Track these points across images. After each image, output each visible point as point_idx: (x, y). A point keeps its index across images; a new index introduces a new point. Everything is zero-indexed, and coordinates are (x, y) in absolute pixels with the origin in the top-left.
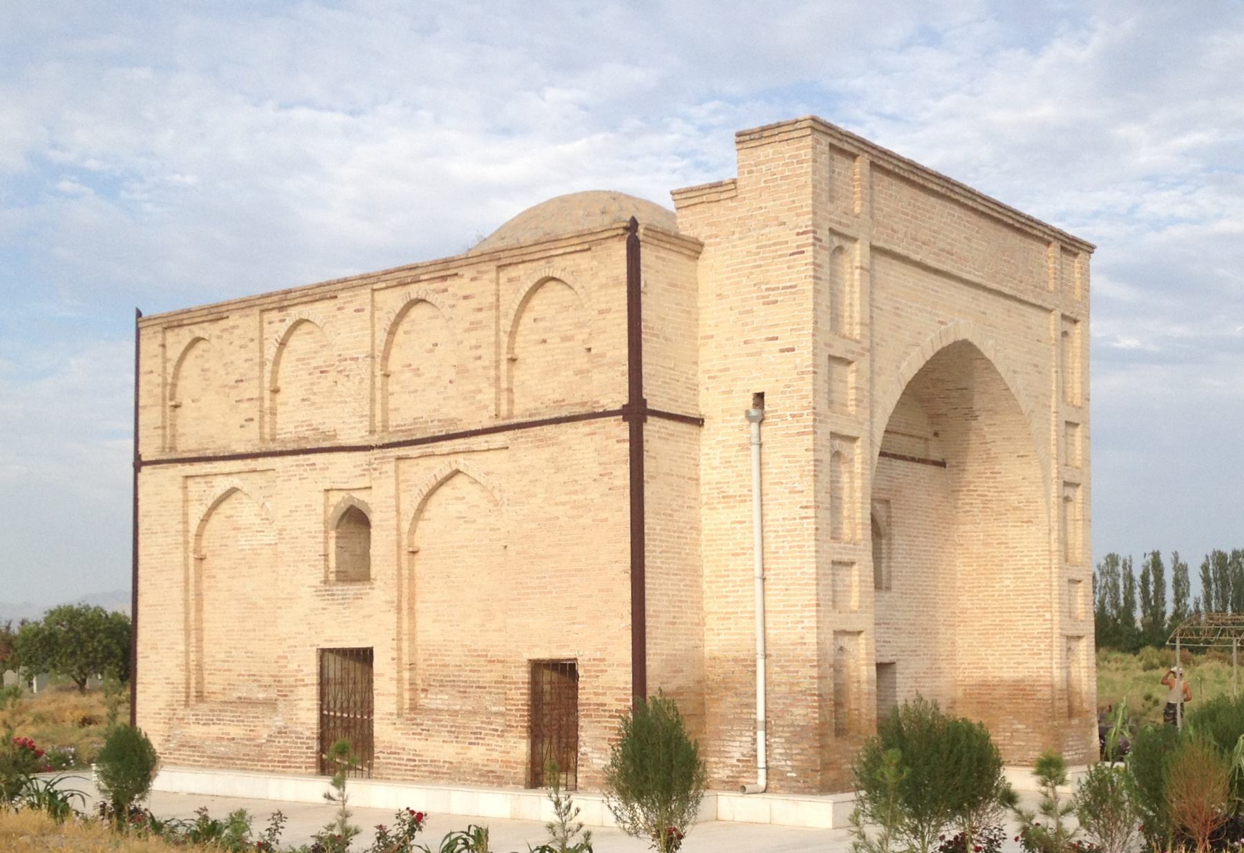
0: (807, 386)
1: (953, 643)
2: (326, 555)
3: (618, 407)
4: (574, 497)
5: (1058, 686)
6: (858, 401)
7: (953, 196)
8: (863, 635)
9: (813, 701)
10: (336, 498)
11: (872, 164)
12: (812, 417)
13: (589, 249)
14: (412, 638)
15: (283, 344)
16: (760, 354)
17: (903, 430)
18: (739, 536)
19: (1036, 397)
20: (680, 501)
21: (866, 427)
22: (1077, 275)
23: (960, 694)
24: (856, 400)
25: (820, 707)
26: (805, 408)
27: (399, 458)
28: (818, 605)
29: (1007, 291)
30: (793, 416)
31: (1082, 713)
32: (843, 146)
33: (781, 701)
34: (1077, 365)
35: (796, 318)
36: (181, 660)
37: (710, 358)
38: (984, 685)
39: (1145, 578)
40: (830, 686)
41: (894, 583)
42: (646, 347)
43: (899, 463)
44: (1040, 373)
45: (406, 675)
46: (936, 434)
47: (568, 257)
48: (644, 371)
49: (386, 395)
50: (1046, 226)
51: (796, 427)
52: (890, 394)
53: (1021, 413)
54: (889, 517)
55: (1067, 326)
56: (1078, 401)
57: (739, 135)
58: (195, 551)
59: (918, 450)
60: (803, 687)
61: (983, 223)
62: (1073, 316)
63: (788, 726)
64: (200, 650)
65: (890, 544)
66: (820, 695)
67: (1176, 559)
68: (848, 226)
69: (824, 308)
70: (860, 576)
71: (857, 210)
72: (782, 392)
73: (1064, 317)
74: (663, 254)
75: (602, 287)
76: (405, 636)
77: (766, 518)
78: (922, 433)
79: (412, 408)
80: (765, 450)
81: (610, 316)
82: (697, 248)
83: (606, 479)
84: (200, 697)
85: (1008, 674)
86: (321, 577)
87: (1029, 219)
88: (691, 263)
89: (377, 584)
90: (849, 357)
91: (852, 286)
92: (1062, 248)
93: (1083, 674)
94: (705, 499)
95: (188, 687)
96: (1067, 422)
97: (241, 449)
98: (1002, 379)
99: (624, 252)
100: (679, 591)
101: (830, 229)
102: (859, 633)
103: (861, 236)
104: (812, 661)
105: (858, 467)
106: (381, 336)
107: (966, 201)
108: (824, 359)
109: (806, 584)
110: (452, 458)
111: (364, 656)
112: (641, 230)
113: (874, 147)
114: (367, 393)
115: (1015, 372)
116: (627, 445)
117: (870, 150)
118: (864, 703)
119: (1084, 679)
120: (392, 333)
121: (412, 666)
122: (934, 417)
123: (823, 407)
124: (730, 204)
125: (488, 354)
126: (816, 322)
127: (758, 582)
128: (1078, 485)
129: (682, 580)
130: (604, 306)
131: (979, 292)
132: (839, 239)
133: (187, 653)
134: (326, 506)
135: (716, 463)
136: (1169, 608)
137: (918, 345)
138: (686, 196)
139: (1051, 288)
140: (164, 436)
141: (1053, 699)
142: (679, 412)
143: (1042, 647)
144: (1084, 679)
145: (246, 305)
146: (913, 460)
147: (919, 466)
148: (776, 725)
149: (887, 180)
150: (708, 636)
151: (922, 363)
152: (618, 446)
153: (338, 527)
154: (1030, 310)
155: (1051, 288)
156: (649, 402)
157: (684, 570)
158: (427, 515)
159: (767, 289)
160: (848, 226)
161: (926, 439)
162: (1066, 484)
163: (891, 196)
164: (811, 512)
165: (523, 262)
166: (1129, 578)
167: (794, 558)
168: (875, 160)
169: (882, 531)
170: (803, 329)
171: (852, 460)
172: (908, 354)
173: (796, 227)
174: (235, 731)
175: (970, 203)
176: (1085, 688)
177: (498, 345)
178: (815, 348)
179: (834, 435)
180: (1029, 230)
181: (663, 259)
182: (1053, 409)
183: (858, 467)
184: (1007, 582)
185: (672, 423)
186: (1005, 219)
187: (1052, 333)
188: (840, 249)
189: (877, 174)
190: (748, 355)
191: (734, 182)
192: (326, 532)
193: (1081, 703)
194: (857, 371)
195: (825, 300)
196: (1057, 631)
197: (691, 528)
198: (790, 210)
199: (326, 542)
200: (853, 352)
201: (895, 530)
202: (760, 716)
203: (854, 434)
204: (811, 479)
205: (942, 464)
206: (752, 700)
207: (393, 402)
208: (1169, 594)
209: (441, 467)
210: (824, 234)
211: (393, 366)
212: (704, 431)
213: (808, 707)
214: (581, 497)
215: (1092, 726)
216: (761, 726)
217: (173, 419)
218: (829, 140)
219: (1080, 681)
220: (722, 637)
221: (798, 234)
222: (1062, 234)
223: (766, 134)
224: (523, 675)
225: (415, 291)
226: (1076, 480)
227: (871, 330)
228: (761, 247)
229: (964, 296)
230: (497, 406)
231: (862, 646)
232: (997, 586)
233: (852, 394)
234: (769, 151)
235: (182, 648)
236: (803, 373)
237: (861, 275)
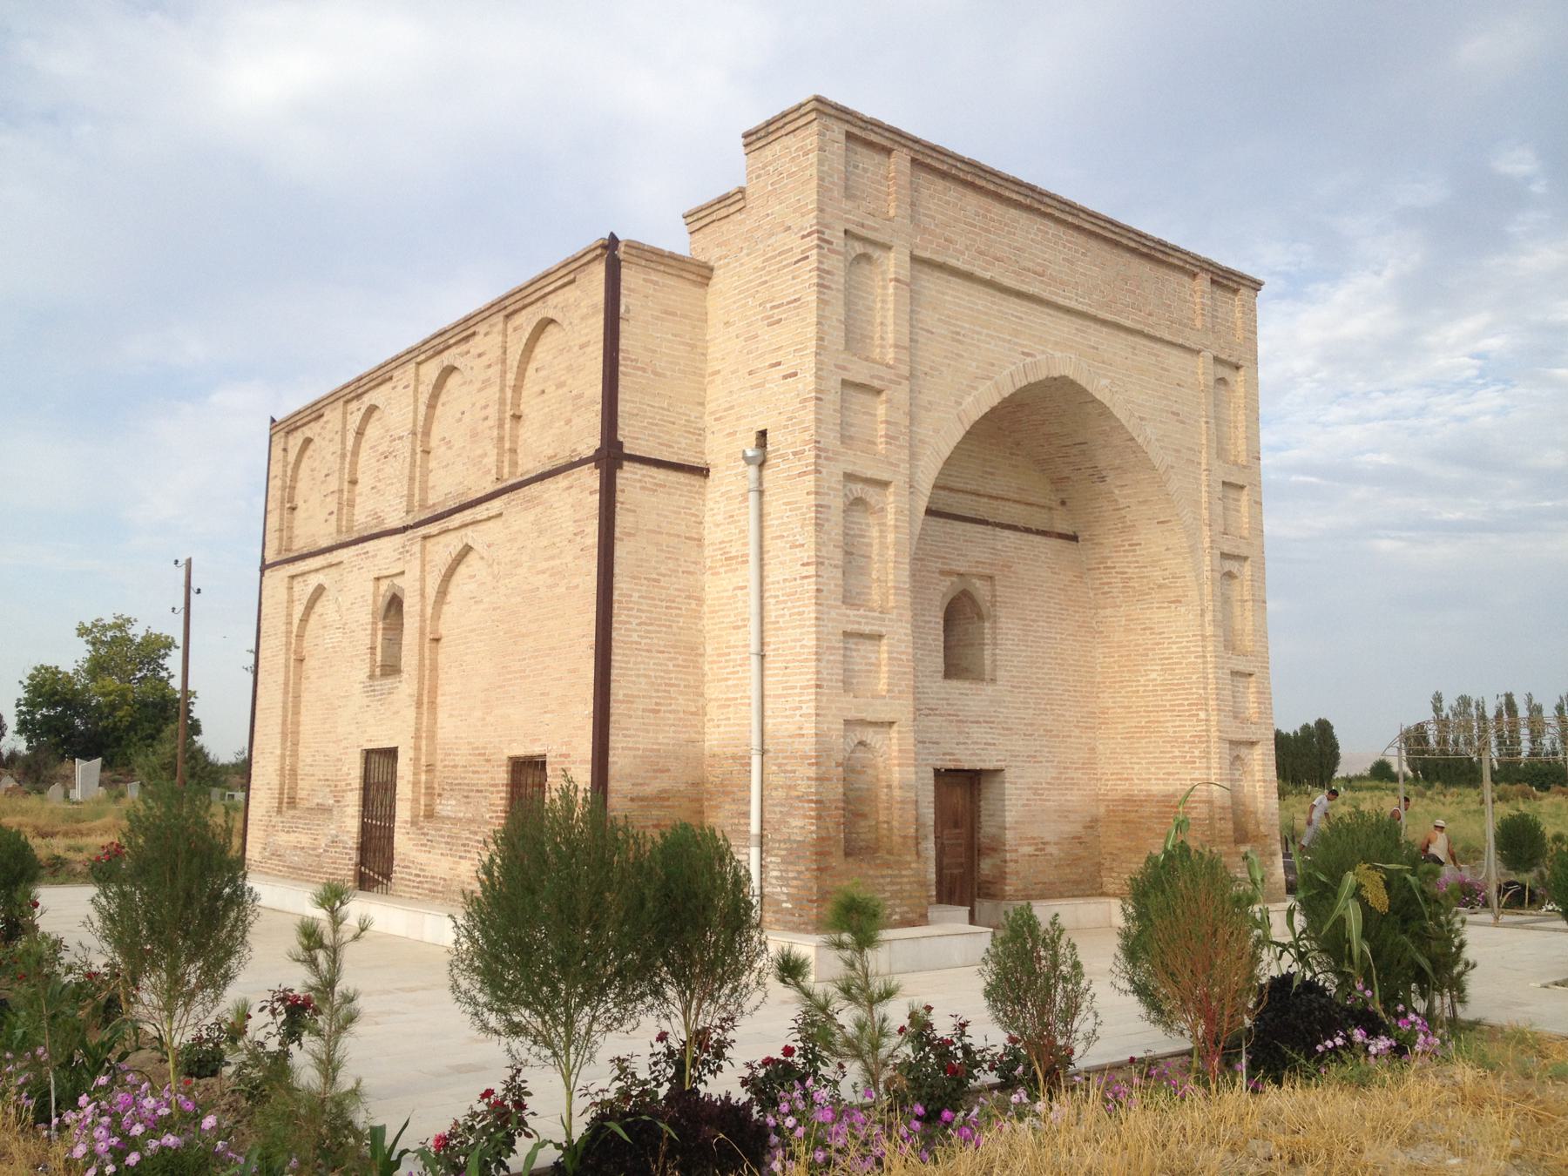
0: (809, 416)
1: (1093, 750)
2: (373, 648)
3: (591, 453)
4: (552, 563)
5: (1218, 803)
6: (890, 439)
7: (1043, 208)
8: (895, 727)
9: (810, 809)
10: (384, 586)
11: (913, 160)
12: (813, 453)
13: (573, 281)
14: (432, 736)
15: (360, 433)
16: (761, 385)
17: (1016, 496)
18: (740, 604)
19: (1178, 451)
20: (671, 565)
21: (904, 468)
22: (1239, 315)
23: (1102, 810)
24: (887, 436)
25: (819, 817)
26: (806, 443)
27: (425, 538)
28: (818, 686)
29: (1128, 323)
30: (795, 454)
31: (1257, 838)
32: (866, 136)
33: (777, 809)
34: (1241, 417)
35: (797, 340)
36: (277, 765)
37: (716, 396)
38: (1129, 800)
39: (1499, 715)
40: (836, 790)
41: (1000, 673)
42: (623, 381)
43: (1007, 533)
44: (1182, 422)
45: (423, 777)
46: (1063, 503)
47: (560, 292)
48: (620, 408)
49: (426, 473)
50: (1188, 254)
51: (799, 466)
52: (943, 434)
53: (1154, 469)
54: (994, 596)
55: (1224, 372)
56: (1242, 460)
57: (746, 136)
58: (296, 652)
59: (1038, 519)
60: (802, 789)
61: (1094, 245)
62: (1233, 360)
63: (785, 841)
64: (295, 754)
65: (994, 628)
66: (817, 802)
67: (1530, 700)
68: (875, 230)
69: (835, 323)
70: (889, 652)
71: (892, 213)
72: (786, 427)
73: (1217, 360)
74: (654, 277)
75: (583, 318)
76: (425, 733)
77: (767, 580)
78: (1042, 501)
79: (445, 485)
80: (767, 498)
81: (590, 349)
82: (705, 272)
83: (578, 538)
84: (292, 803)
85: (1157, 788)
86: (366, 671)
87: (1160, 242)
88: (697, 291)
89: (405, 676)
90: (876, 383)
91: (884, 301)
92: (1213, 282)
93: (1259, 788)
94: (708, 563)
95: (281, 793)
96: (1224, 483)
97: (324, 544)
98: (1122, 426)
99: (603, 275)
100: (667, 672)
101: (846, 232)
102: (891, 724)
103: (896, 242)
104: (810, 757)
105: (890, 519)
106: (422, 409)
107: (1063, 216)
108: (834, 383)
109: (806, 660)
110: (463, 531)
111: (392, 754)
112: (622, 248)
113: (916, 141)
114: (407, 472)
115: (1142, 419)
116: (597, 496)
117: (910, 143)
118: (896, 813)
119: (1260, 796)
120: (431, 406)
121: (430, 768)
122: (1058, 482)
123: (832, 440)
124: (738, 217)
125: (493, 411)
126: (821, 339)
127: (755, 660)
128: (1245, 559)
129: (670, 659)
130: (584, 340)
131: (1087, 323)
132: (862, 247)
133: (283, 757)
134: (375, 595)
135: (719, 518)
136: (1525, 747)
137: (990, 378)
138: (699, 218)
139: (1199, 326)
140: (281, 539)
141: (1211, 818)
142: (674, 459)
143: (1197, 753)
144: (1260, 796)
145: (333, 397)
146: (1028, 530)
147: (1038, 538)
148: (773, 840)
149: (940, 184)
150: (709, 728)
151: (996, 401)
152: (590, 499)
153: (385, 618)
154: (1166, 349)
155: (1199, 326)
156: (626, 445)
157: (673, 647)
158: (449, 598)
159: (773, 308)
160: (875, 230)
161: (1050, 509)
162: (1225, 556)
163: (948, 203)
164: (811, 570)
165: (524, 307)
166: (1483, 717)
167: (794, 628)
168: (920, 157)
169: (984, 611)
170: (806, 348)
171: (882, 510)
172: (975, 388)
173: (802, 229)
174: (305, 840)
175: (1070, 219)
176: (1261, 806)
177: (502, 402)
178: (818, 369)
179: (850, 477)
180: (1160, 256)
181: (656, 283)
182: (1204, 466)
183: (890, 519)
184: (1153, 675)
185: (662, 471)
186: (1125, 241)
187: (1201, 378)
188: (865, 258)
189: (924, 178)
190: (752, 387)
191: (741, 191)
192: (374, 623)
193: (1258, 824)
194: (888, 401)
195: (837, 311)
196: (1214, 734)
197: (688, 597)
198: (795, 211)
199: (374, 634)
200: (881, 379)
201: (1002, 612)
202: (755, 828)
203: (885, 477)
204: (812, 528)
205: (1074, 538)
206: (744, 808)
207: (432, 479)
208: (1524, 733)
209: (453, 543)
210: (837, 237)
211: (434, 441)
212: (709, 482)
213: (805, 816)
214: (558, 562)
215: (1273, 854)
216: (755, 841)
217: (291, 521)
218: (847, 127)
219: (1255, 797)
220: (722, 729)
221: (803, 237)
222: (1211, 264)
223: (772, 128)
224: (502, 776)
225: (447, 358)
226: (1243, 552)
227: (912, 355)
228: (766, 260)
229: (1065, 327)
230: (499, 468)
231: (894, 741)
232: (1142, 680)
233: (882, 429)
234: (777, 147)
235: (278, 752)
236: (805, 400)
237: (896, 288)
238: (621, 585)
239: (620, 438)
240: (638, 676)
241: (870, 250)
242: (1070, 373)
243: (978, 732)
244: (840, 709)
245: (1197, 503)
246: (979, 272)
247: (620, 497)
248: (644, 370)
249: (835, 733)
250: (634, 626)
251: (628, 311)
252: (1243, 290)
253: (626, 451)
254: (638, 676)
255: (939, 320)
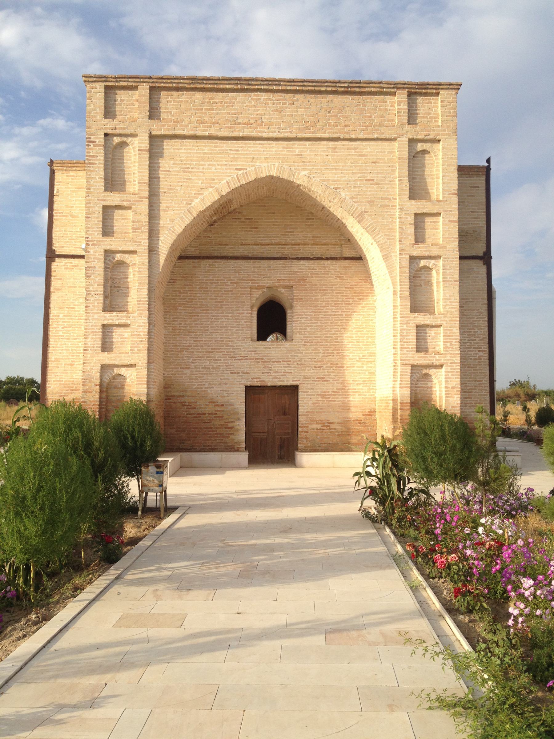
6: (135, 230)
7: (251, 87)
68: (124, 129)
74: (71, 173)
103: (138, 132)
115: (336, 188)
172: (202, 194)
238: (53, 312)
239: (54, 248)
240: (62, 350)
241: (125, 139)
242: (274, 173)
243: (276, 367)
244: (98, 360)
245: (392, 230)
246: (199, 133)
247: (53, 274)
248: (66, 216)
249: (94, 372)
250: (60, 329)
251: (58, 192)
252: (442, 92)
253: (57, 253)
254: (62, 350)
255: (174, 164)
